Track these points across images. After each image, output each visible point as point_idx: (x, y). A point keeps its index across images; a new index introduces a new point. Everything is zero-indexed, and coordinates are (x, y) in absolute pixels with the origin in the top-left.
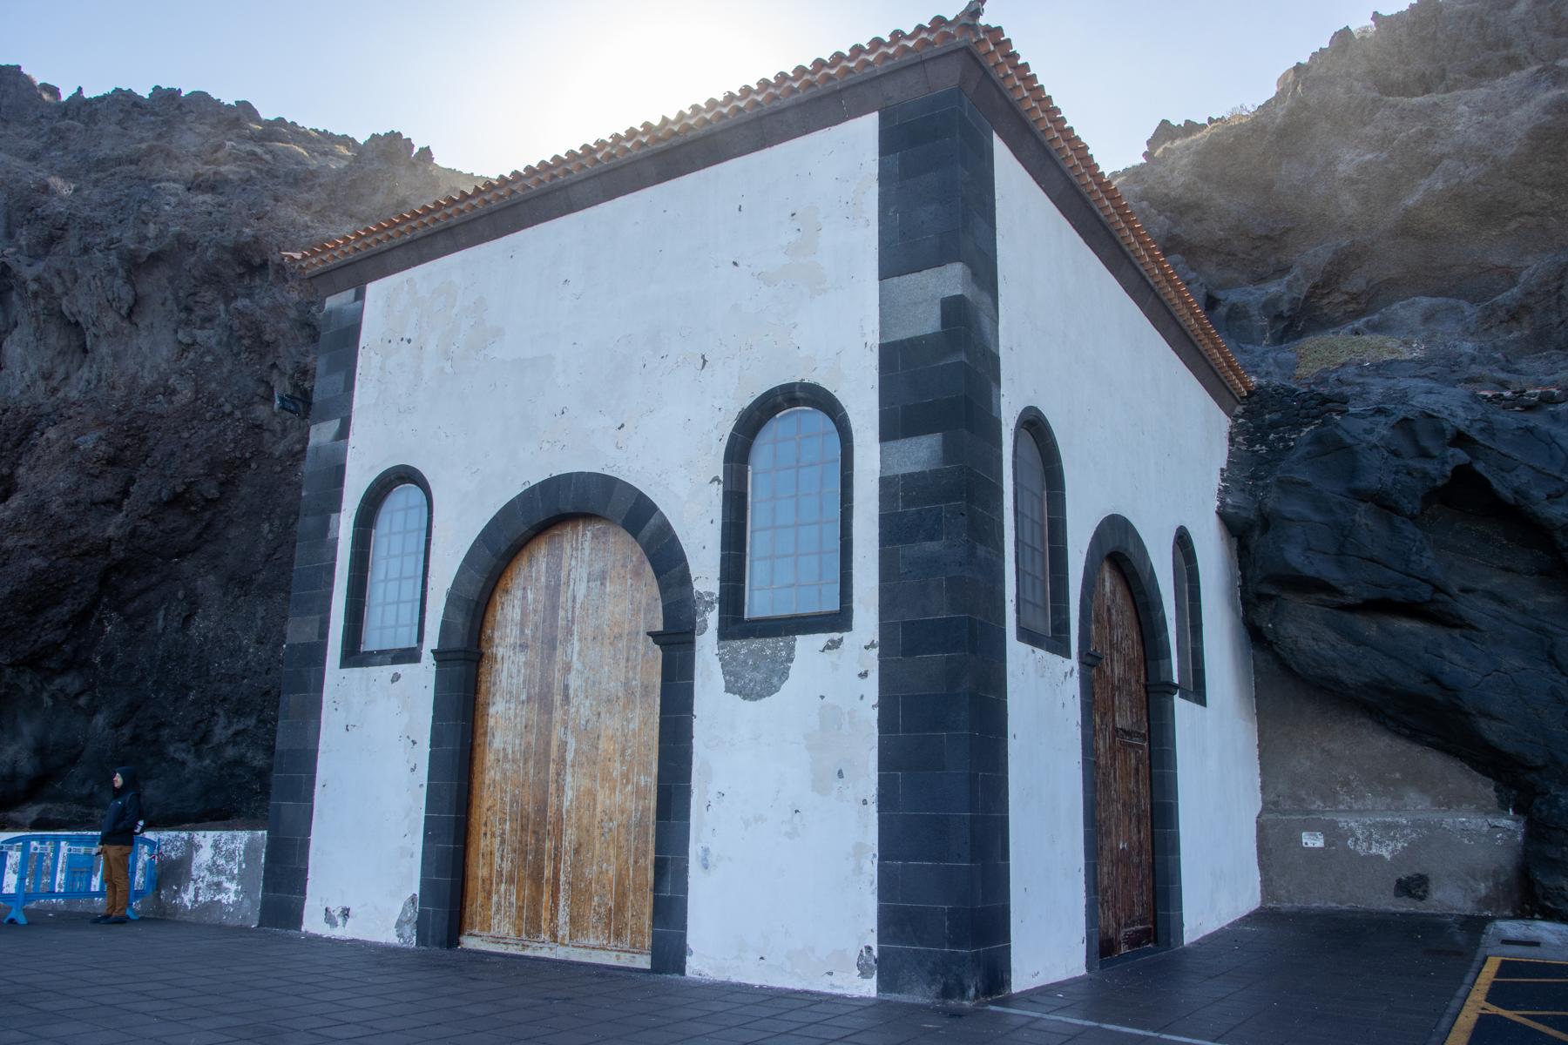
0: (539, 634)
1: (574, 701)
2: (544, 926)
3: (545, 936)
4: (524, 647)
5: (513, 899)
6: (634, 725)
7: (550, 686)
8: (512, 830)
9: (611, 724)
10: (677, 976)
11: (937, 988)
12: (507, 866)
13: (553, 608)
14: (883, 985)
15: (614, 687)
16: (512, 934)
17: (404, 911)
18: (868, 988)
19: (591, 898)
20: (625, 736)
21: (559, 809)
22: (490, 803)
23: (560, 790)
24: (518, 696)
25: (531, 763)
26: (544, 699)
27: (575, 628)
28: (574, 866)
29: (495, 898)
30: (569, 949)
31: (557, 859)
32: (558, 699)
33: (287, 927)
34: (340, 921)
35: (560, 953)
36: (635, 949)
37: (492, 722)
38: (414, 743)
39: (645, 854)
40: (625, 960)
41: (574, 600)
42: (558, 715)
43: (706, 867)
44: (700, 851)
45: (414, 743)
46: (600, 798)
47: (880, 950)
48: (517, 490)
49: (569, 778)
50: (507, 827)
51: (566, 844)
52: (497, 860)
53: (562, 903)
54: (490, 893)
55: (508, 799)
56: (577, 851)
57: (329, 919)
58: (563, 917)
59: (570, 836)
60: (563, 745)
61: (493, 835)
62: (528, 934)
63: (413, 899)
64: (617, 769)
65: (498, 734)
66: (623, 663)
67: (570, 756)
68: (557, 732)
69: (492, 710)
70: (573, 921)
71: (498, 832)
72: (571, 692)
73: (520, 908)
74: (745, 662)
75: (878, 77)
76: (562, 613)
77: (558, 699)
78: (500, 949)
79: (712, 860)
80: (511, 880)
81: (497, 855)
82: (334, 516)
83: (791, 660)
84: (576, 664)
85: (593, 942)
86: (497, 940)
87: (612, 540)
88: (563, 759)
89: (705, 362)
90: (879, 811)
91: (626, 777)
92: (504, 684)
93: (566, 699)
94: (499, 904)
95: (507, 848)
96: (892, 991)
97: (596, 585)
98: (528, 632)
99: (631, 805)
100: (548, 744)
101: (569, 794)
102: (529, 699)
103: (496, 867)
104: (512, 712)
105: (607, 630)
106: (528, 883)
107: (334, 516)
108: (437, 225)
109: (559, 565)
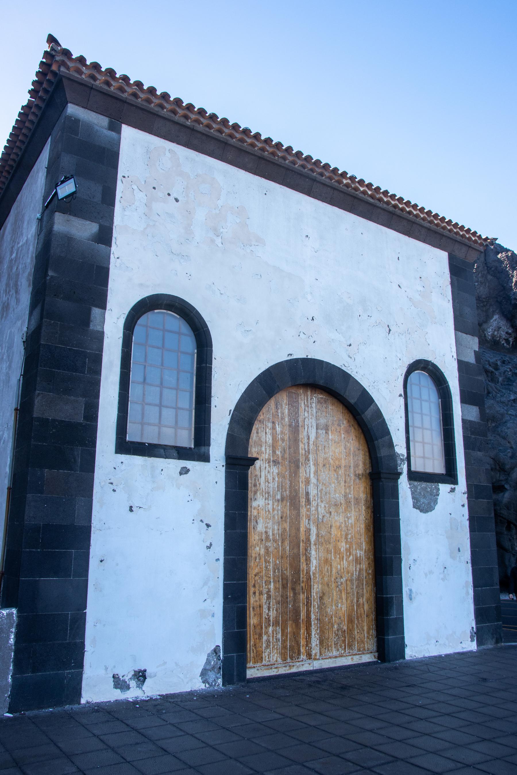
0: (287, 456)
1: (314, 503)
2: (302, 650)
3: (303, 657)
4: (276, 462)
5: (279, 636)
6: (352, 521)
7: (297, 492)
8: (275, 588)
9: (338, 519)
10: (401, 661)
11: (494, 640)
12: (273, 614)
13: (295, 440)
14: (479, 644)
15: (338, 497)
16: (280, 660)
17: (208, 662)
18: (473, 646)
19: (333, 626)
20: (347, 527)
21: (308, 572)
22: (256, 570)
23: (308, 560)
24: (274, 497)
25: (287, 543)
26: (293, 500)
27: (311, 456)
28: (320, 608)
29: (265, 638)
30: (321, 661)
31: (308, 604)
32: (303, 501)
33: (60, 703)
34: (133, 684)
35: (316, 665)
36: (362, 652)
37: (255, 513)
38: (208, 526)
39: (362, 596)
40: (356, 660)
41: (308, 439)
42: (303, 511)
43: (411, 599)
44: (408, 591)
45: (208, 526)
46: (334, 564)
47: (477, 628)
48: (283, 357)
49: (313, 552)
50: (272, 586)
51: (314, 594)
52: (265, 610)
53: (313, 633)
54: (260, 635)
55: (271, 567)
56: (321, 598)
57: (119, 684)
58: (315, 641)
59: (316, 589)
60: (308, 531)
61: (261, 593)
62: (291, 658)
63: (216, 651)
64: (343, 546)
65: (261, 521)
66: (343, 484)
67: (313, 538)
68: (304, 523)
69: (254, 504)
70: (321, 642)
71: (265, 591)
72: (311, 497)
73: (284, 641)
74: (420, 493)
75: (456, 241)
76: (301, 445)
77: (303, 501)
78: (273, 672)
79: (413, 595)
80: (276, 623)
81: (265, 607)
82: (96, 311)
83: (438, 495)
84: (313, 480)
85: (335, 653)
86: (270, 666)
87: (330, 407)
88: (308, 540)
89: (390, 330)
90: (472, 566)
91: (348, 550)
92: (263, 486)
93: (308, 501)
94: (268, 641)
95: (273, 602)
96: (484, 644)
97: (322, 432)
98: (278, 453)
99: (352, 568)
100: (298, 529)
101: (314, 562)
102: (282, 499)
103: (265, 615)
104: (270, 507)
105: (331, 462)
106: (290, 623)
107: (96, 311)
108: (218, 134)
109: (297, 413)
